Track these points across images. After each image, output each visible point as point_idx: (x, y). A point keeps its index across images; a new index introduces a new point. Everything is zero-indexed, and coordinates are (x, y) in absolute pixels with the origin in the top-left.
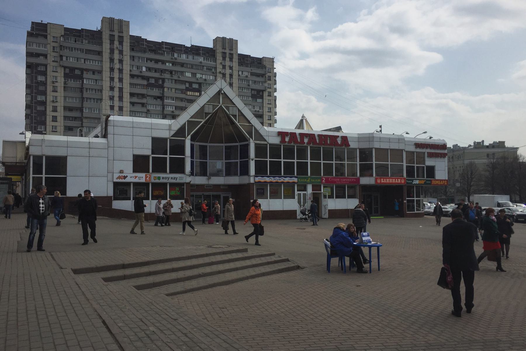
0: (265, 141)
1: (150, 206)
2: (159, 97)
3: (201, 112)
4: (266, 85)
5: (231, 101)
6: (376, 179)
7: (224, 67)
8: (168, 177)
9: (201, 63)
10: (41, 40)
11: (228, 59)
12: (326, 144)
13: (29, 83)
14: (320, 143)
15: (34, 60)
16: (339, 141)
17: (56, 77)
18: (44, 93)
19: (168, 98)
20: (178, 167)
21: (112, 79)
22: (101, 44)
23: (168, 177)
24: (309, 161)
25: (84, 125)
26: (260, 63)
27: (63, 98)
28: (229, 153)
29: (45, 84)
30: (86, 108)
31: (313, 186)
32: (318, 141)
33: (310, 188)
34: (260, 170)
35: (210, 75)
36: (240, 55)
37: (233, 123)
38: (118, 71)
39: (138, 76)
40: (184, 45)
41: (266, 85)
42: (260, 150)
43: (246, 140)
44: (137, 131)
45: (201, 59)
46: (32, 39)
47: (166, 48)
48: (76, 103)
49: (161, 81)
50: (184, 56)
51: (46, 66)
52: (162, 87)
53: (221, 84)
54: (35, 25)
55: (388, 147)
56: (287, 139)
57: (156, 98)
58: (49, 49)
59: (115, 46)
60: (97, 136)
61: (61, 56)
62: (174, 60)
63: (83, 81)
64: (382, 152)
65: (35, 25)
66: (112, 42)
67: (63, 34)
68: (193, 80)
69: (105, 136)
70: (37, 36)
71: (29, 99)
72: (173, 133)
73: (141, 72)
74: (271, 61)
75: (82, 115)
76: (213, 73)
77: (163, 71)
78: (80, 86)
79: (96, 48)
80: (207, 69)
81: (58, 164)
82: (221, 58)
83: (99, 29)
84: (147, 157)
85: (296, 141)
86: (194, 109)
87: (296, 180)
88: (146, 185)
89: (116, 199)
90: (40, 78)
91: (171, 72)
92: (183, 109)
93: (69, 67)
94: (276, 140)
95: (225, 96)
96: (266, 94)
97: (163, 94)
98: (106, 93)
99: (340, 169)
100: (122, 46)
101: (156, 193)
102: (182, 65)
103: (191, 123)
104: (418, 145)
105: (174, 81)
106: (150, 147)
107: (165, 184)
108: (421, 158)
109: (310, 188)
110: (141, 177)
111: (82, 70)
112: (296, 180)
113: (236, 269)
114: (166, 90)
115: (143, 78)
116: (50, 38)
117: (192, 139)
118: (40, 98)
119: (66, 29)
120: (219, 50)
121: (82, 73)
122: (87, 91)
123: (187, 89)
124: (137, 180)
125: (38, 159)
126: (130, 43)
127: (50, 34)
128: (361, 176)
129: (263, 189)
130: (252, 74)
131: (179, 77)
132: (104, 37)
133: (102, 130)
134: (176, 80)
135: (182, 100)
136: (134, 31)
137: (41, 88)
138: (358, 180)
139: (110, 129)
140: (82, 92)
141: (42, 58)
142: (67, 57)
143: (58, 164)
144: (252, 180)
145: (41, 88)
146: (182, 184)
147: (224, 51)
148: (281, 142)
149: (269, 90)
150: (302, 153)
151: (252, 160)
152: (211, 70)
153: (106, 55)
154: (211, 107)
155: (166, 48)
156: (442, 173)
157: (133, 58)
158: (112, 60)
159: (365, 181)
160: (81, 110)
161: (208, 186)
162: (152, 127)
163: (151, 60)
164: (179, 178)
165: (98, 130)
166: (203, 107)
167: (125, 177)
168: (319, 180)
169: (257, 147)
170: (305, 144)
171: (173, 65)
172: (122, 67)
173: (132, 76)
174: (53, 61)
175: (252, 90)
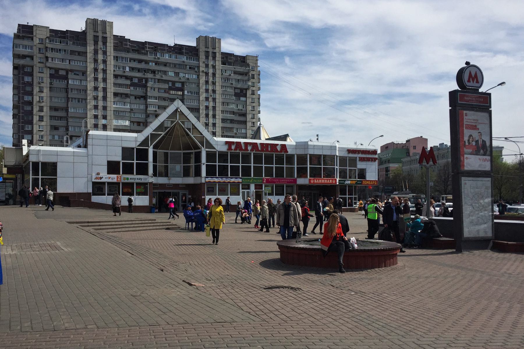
0: (215, 148)
1: (124, 200)
2: (142, 97)
3: (161, 127)
4: (250, 84)
5: (186, 117)
6: (310, 180)
7: (207, 66)
8: (134, 178)
9: (184, 62)
10: (26, 42)
11: (210, 58)
12: (267, 150)
13: (16, 84)
14: (262, 150)
15: (22, 62)
16: (279, 148)
17: (42, 78)
18: (31, 94)
19: (151, 97)
20: (143, 170)
21: (96, 79)
22: (85, 45)
23: (134, 178)
24: (252, 165)
25: (69, 124)
26: (244, 62)
27: (49, 98)
28: (187, 159)
29: (31, 84)
30: (71, 108)
31: (255, 185)
32: (260, 149)
33: (252, 187)
34: (211, 172)
35: (193, 74)
36: (223, 54)
37: (188, 135)
38: (102, 71)
39: (121, 76)
40: (167, 45)
41: (250, 84)
42: (211, 156)
43: (199, 148)
44: (112, 140)
45: (184, 59)
46: (18, 41)
47: (149, 48)
48: (60, 102)
49: (144, 80)
50: (167, 56)
51: (32, 67)
52: (145, 86)
53: (178, 104)
54: (21, 27)
55: (321, 154)
56: (233, 147)
57: (140, 97)
58: (35, 51)
59: (99, 47)
60: (79, 146)
61: (47, 58)
62: (157, 60)
63: (68, 82)
64: (316, 158)
65: (21, 27)
66: (96, 43)
67: (48, 35)
68: (176, 79)
69: (86, 146)
70: (23, 38)
71: (17, 99)
72: (138, 143)
73: (124, 72)
74: (255, 59)
75: (67, 115)
76: (196, 72)
77: (149, 70)
78: (65, 86)
79: (79, 49)
80: (190, 68)
81: (50, 168)
82: (204, 57)
83: (84, 29)
84: (119, 162)
85: (241, 149)
86: (156, 123)
87: (240, 180)
88: (118, 184)
89: (94, 194)
90: (27, 79)
91: (154, 72)
92: (165, 108)
93: (56, 70)
94: (224, 149)
95: (182, 113)
96: (249, 93)
97: (146, 93)
98: (90, 94)
99: (280, 171)
100: (106, 47)
101: (126, 190)
102: (165, 65)
103: (153, 136)
104: (350, 151)
105: (157, 81)
106: (121, 155)
107: (132, 184)
108: (353, 162)
109: (252, 187)
110: (114, 178)
111: (67, 71)
112: (240, 180)
113: (144, 226)
114: (149, 89)
115: (127, 78)
116: (36, 41)
117: (154, 148)
118: (27, 98)
119: (52, 31)
120: (202, 49)
121: (67, 73)
122: (72, 92)
123: (170, 89)
124: (110, 180)
125: (36, 165)
126: (114, 43)
127: (36, 36)
128: (297, 177)
129: (213, 188)
130: (235, 73)
131: (162, 77)
132: (88, 38)
133: (83, 141)
134: (159, 80)
135: (164, 99)
136: (117, 31)
137: (28, 89)
138: (295, 181)
139: (89, 141)
140: (67, 92)
141: (28, 59)
142: (52, 58)
143: (50, 168)
144: (203, 181)
145: (28, 89)
146: (146, 184)
147: (207, 50)
148: (228, 149)
149: (252, 88)
150: (246, 158)
151: (204, 164)
152: (194, 69)
153: (90, 55)
154: (170, 122)
155: (149, 48)
156: (372, 174)
157: (116, 58)
158: (96, 61)
159: (301, 181)
160: (66, 110)
161: (169, 185)
162: (122, 139)
163: (134, 60)
164: (142, 179)
165: (80, 141)
166: (162, 123)
167: (101, 178)
168: (261, 181)
169: (208, 154)
170: (249, 151)
171: (156, 64)
172: (106, 67)
173: (116, 76)
174: (39, 62)
175: (235, 88)
